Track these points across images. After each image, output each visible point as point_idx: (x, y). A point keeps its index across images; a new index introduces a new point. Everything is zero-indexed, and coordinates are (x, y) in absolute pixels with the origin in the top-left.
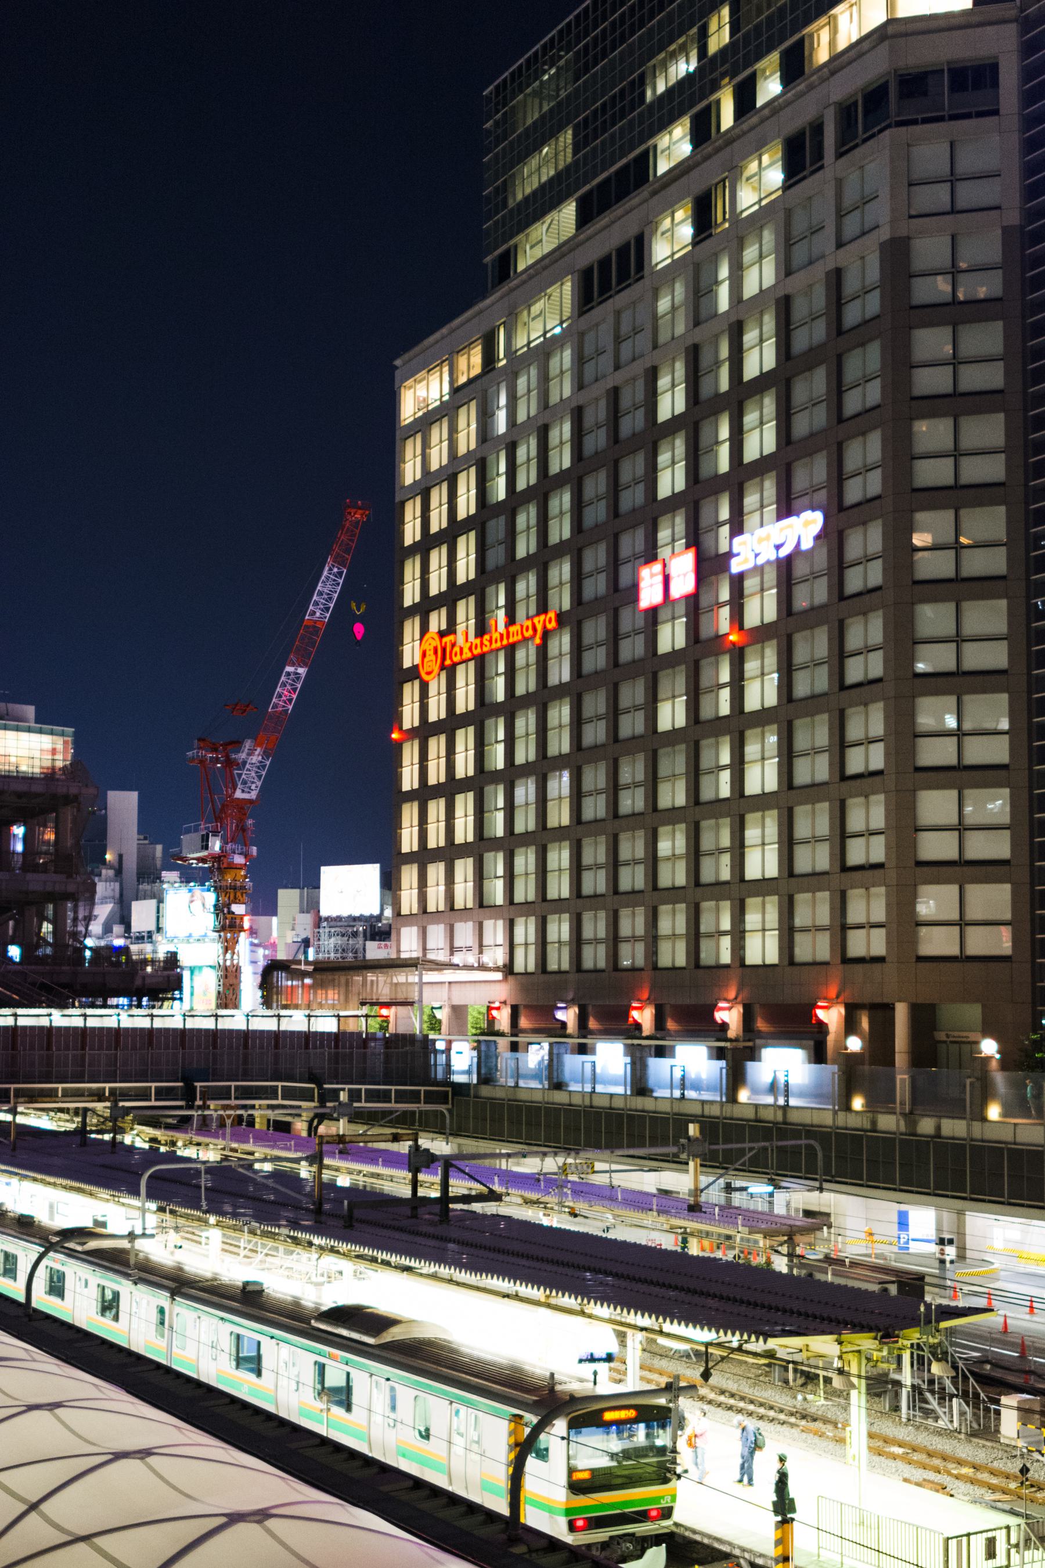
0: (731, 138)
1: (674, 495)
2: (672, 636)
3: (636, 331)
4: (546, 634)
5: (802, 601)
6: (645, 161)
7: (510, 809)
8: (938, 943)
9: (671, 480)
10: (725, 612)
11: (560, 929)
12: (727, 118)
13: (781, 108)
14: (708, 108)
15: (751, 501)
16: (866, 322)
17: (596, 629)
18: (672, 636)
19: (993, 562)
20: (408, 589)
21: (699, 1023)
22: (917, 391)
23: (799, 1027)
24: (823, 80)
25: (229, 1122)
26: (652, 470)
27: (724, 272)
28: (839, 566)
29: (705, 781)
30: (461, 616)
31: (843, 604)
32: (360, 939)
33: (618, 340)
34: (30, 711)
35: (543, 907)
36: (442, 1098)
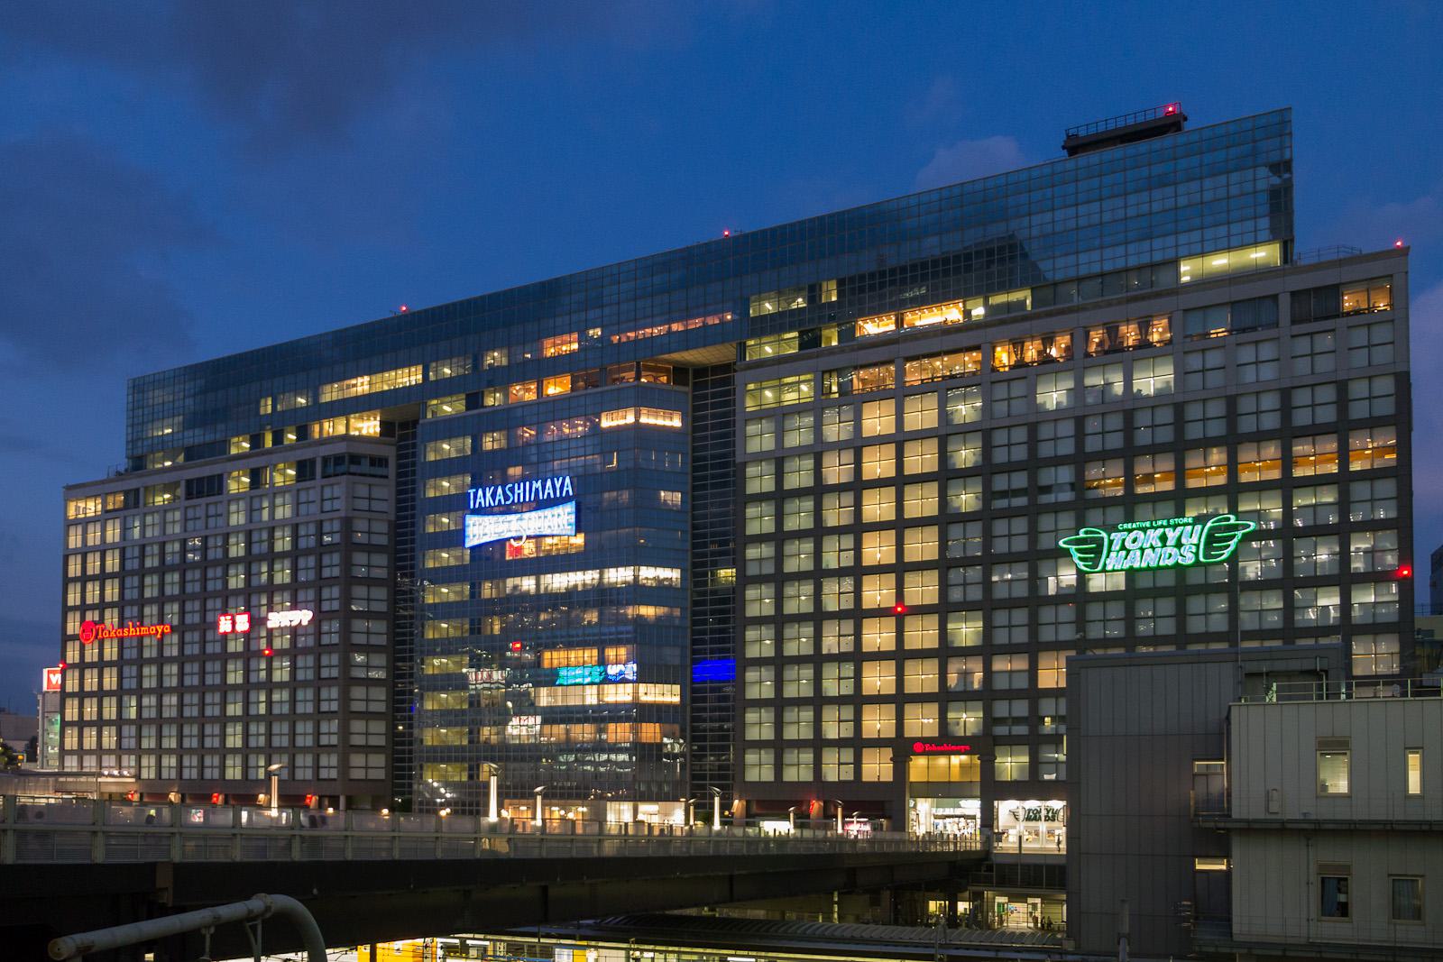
0: (269, 452)
2: (235, 646)
6: (225, 444)
8: (357, 774)
15: (277, 599)
27: (266, 504)
28: (319, 634)
31: (319, 649)
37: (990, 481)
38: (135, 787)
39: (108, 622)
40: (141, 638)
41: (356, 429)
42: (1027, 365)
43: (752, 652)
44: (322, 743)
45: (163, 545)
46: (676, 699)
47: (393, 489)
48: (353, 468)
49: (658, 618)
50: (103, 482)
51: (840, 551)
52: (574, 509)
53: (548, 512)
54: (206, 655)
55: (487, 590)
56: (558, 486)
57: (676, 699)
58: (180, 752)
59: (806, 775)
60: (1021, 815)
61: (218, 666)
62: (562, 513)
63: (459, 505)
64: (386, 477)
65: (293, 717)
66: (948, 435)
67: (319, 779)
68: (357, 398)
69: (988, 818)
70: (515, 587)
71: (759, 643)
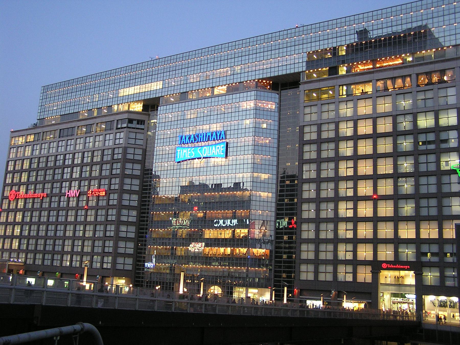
37: (418, 158)
39: (21, 191)
41: (132, 108)
42: (433, 84)
44: (110, 204)
50: (27, 130)
51: (346, 209)
59: (329, 278)
60: (437, 303)
61: (59, 256)
64: (143, 129)
66: (397, 115)
67: (102, 268)
69: (420, 304)
71: (307, 252)
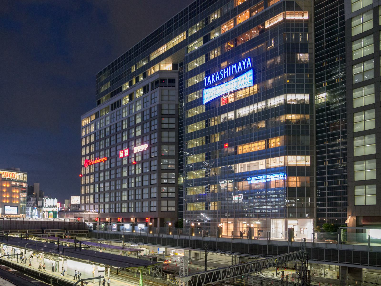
0: (135, 86)
1: (139, 136)
2: (125, 162)
3: (114, 117)
4: (105, 161)
5: (145, 158)
6: (121, 88)
7: (99, 188)
8: (164, 209)
9: (125, 138)
10: (133, 159)
11: (107, 206)
12: (134, 83)
13: (143, 82)
14: (131, 81)
15: (137, 142)
16: (155, 116)
17: (113, 160)
18: (125, 162)
19: (173, 154)
20: (83, 152)
21: (128, 220)
22: (163, 127)
23: (143, 221)
24: (135, 87)
25: (48, 236)
26: (122, 136)
27: (134, 107)
28: (150, 153)
29: (130, 184)
30: (91, 157)
31: (151, 159)
32: (78, 208)
33: (117, 116)
34: (19, 169)
35: (104, 203)
36: (87, 232)
38: (98, 216)
40: (100, 163)
43: (359, 177)
44: (151, 184)
45: (105, 129)
46: (308, 164)
47: (177, 91)
48: (162, 84)
49: (298, 121)
52: (252, 73)
53: (239, 78)
54: (116, 165)
55: (213, 123)
56: (244, 64)
57: (308, 164)
58: (110, 202)
62: (246, 77)
63: (201, 86)
65: (142, 187)
67: (150, 211)
68: (163, 54)
70: (225, 118)
